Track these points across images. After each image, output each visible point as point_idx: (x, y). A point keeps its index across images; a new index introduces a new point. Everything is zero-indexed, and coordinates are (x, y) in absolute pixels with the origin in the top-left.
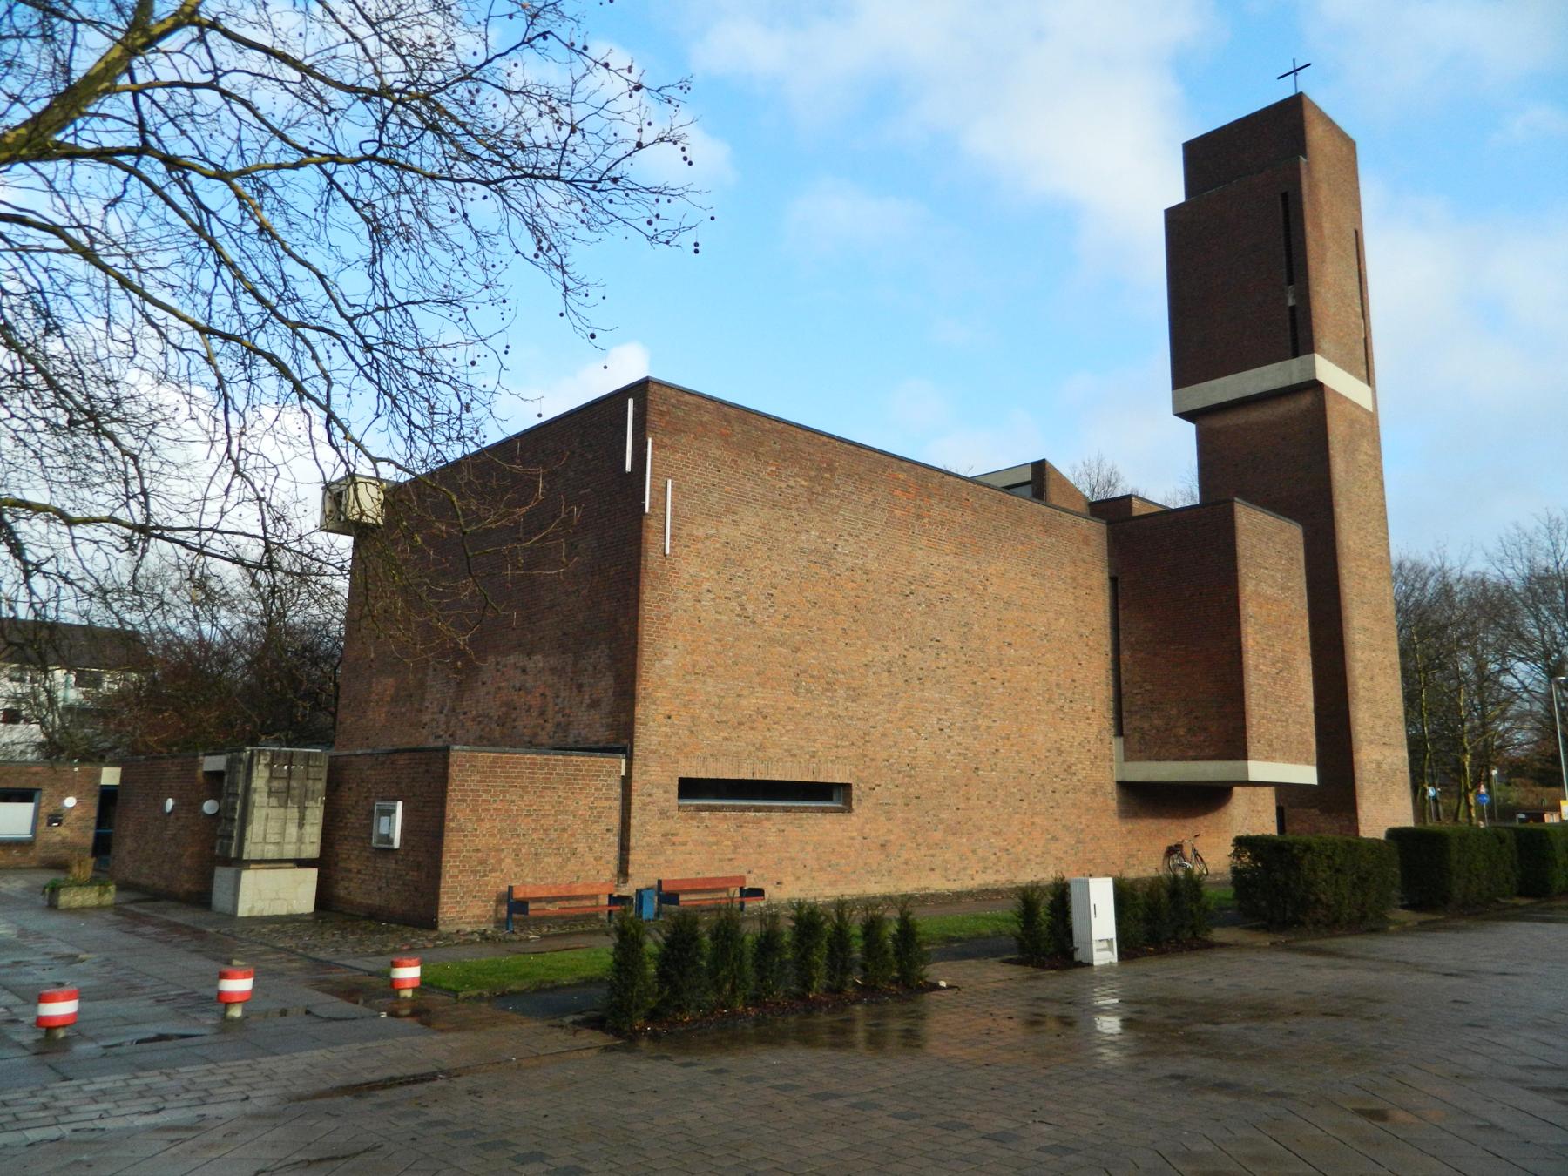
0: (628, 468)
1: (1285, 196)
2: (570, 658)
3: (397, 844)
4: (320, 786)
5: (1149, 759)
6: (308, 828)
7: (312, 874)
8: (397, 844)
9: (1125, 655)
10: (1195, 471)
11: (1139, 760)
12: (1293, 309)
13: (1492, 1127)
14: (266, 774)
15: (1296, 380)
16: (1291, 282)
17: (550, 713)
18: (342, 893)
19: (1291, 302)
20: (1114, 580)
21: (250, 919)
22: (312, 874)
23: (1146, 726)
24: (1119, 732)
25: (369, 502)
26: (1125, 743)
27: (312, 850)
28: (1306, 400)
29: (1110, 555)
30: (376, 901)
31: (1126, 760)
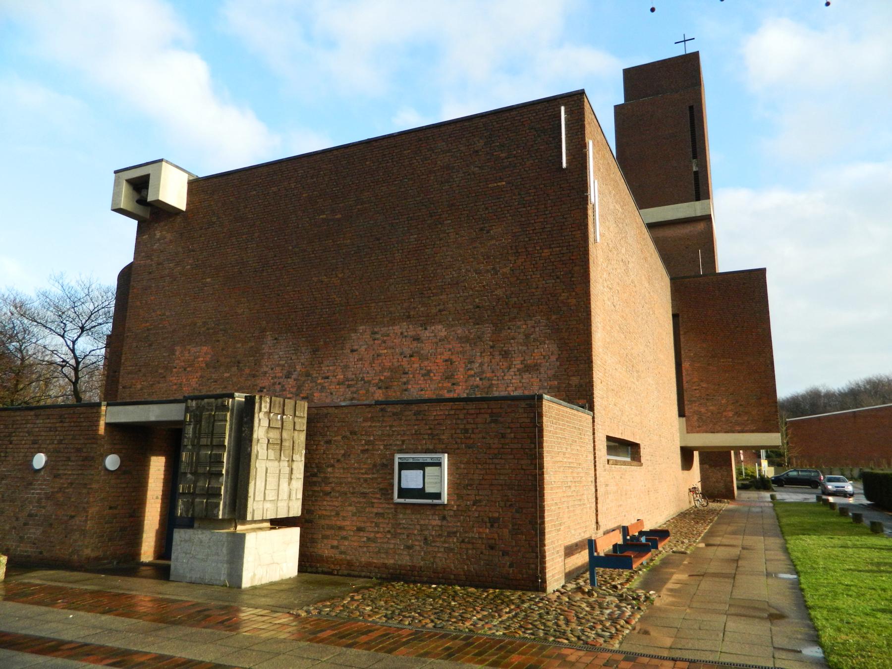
0: (564, 165)
1: (691, 108)
2: (488, 329)
3: (445, 499)
4: (301, 438)
5: (706, 432)
6: (293, 482)
7: (294, 534)
8: (445, 499)
9: (686, 365)
10: (591, 270)
11: (698, 432)
12: (696, 173)
13: (264, 596)
14: (265, 423)
15: (699, 214)
16: (695, 157)
17: (460, 376)
18: (327, 553)
19: (695, 169)
20: (675, 316)
21: (254, 588)
22: (294, 534)
23: (703, 410)
24: (681, 414)
25: (173, 191)
26: (687, 421)
27: (296, 510)
28: (701, 226)
29: (672, 300)
30: (405, 560)
31: (688, 432)
